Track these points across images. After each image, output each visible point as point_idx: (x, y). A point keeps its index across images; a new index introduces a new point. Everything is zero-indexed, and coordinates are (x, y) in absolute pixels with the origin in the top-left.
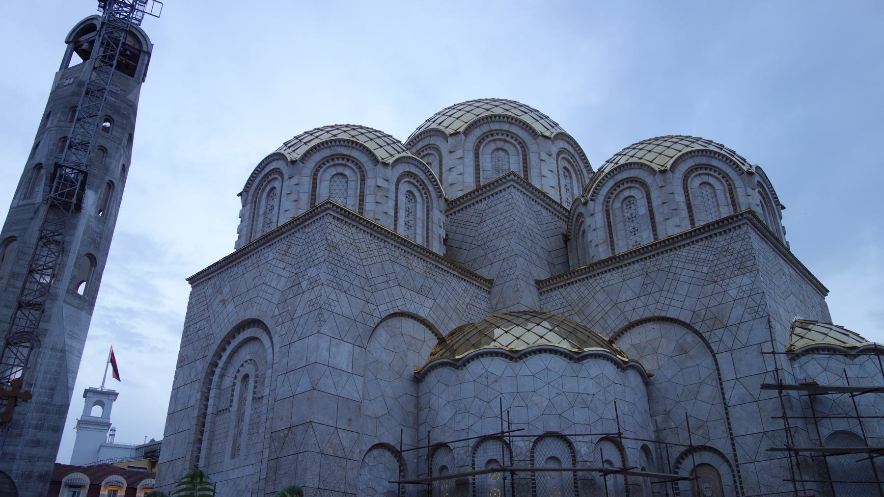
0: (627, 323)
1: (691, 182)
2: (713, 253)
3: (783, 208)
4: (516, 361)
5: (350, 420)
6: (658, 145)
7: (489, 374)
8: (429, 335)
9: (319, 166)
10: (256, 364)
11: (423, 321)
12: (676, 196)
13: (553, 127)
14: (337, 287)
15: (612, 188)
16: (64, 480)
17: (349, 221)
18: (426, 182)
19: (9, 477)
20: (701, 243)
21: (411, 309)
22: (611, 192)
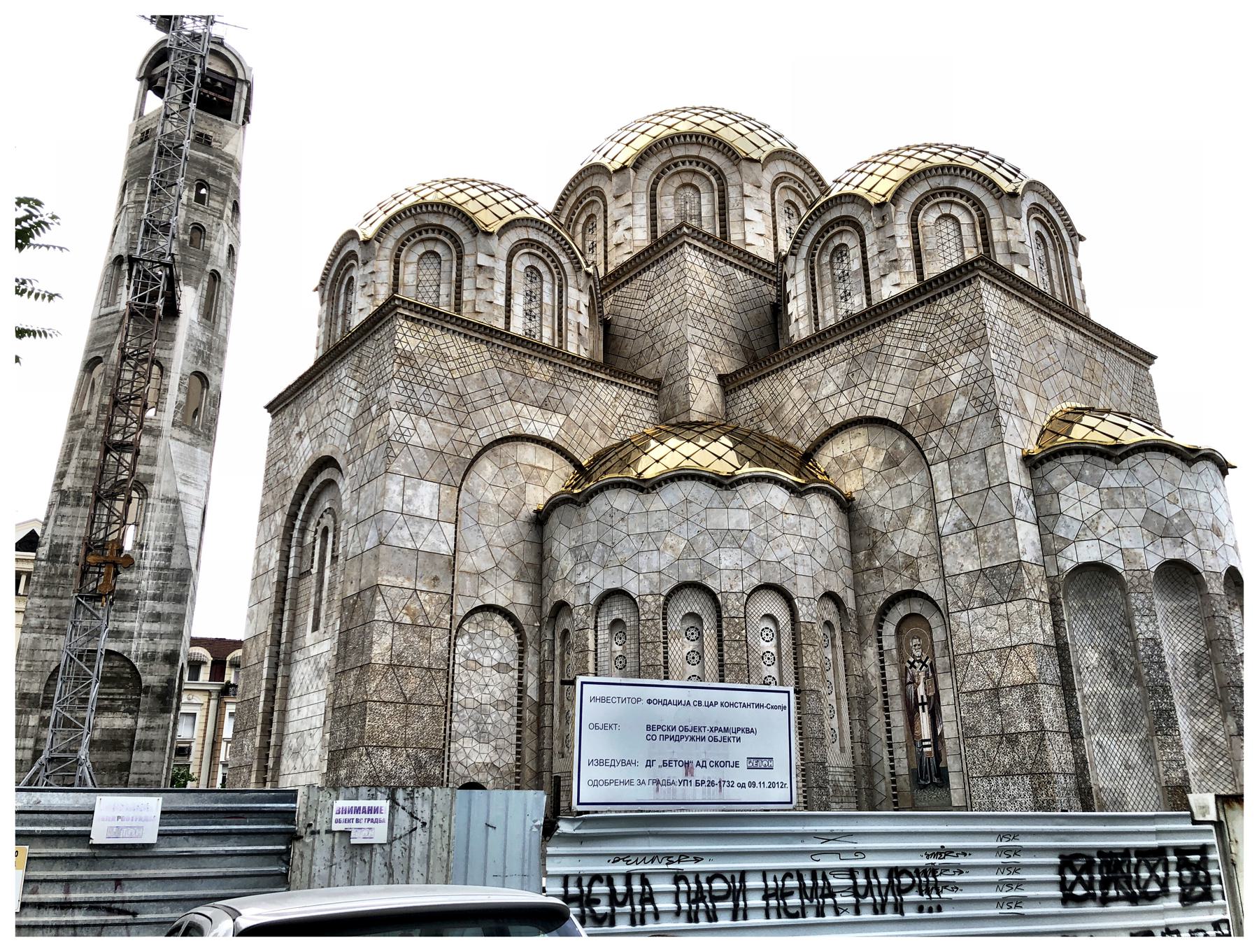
0: (825, 429)
1: (924, 217)
2: (935, 322)
3: (1081, 238)
4: (648, 493)
5: (436, 579)
6: (910, 157)
7: (614, 511)
8: (559, 460)
9: (402, 244)
10: (334, 516)
11: (550, 445)
12: (898, 239)
13: (776, 139)
14: (412, 411)
15: (972, 195)
16: (228, 658)
17: (430, 320)
18: (556, 251)
19: (128, 660)
20: (921, 309)
21: (530, 430)
22: (816, 240)
